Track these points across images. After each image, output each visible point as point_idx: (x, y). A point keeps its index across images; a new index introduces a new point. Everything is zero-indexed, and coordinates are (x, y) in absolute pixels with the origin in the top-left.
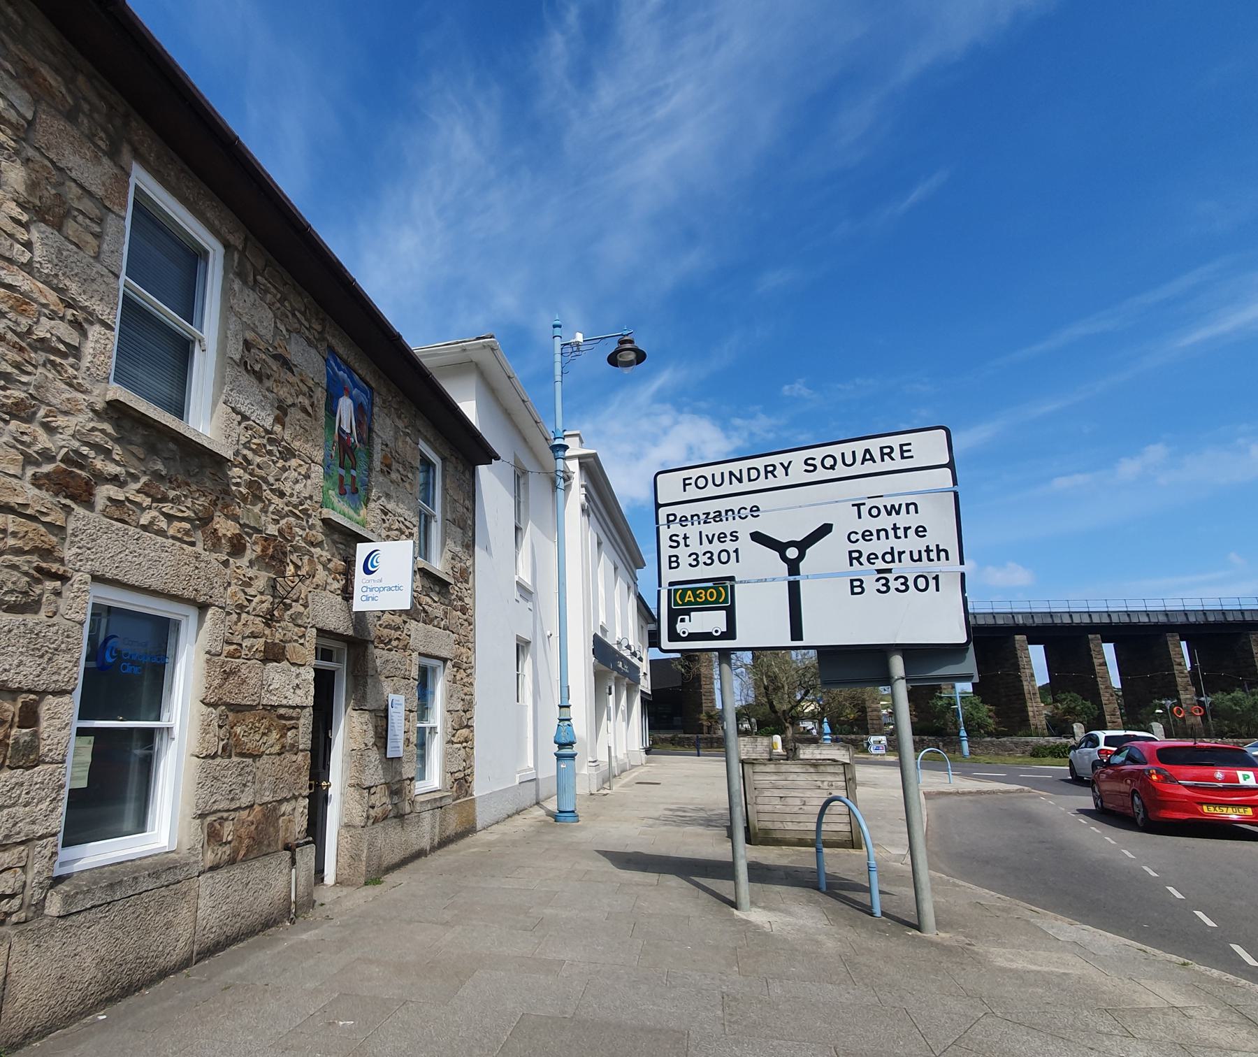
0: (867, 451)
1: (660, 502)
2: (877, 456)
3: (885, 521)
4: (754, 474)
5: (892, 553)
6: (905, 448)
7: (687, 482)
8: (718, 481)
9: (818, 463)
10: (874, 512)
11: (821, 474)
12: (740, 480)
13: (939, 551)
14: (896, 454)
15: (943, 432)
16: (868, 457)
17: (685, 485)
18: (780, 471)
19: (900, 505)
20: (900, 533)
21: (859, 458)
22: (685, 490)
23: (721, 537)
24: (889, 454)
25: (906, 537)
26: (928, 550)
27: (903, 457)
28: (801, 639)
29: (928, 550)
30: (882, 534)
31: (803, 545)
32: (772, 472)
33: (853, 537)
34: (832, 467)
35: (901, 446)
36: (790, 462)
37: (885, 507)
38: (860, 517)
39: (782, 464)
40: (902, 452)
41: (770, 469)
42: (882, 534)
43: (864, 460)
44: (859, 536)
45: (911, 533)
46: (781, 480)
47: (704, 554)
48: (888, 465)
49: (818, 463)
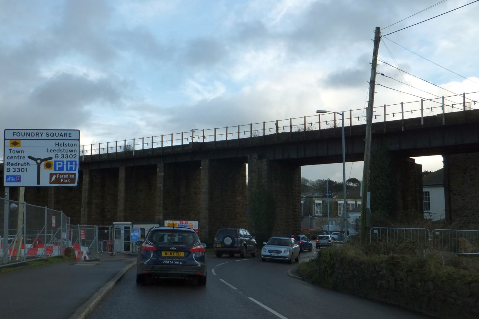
0: (61, 133)
1: (6, 138)
2: (63, 135)
3: (16, 155)
4: (33, 135)
5: (17, 164)
6: (70, 134)
7: (14, 133)
8: (23, 135)
9: (49, 134)
10: (14, 152)
11: (50, 138)
12: (29, 136)
13: (27, 163)
14: (68, 135)
15: (78, 131)
16: (61, 135)
17: (13, 134)
18: (40, 135)
19: (20, 151)
20: (19, 158)
21: (59, 135)
22: (13, 136)
23: (71, 151)
24: (66, 135)
25: (20, 159)
26: (25, 163)
27: (69, 136)
28: (40, 184)
29: (25, 163)
30: (15, 158)
31: (35, 160)
32: (38, 135)
33: (8, 158)
34: (53, 136)
35: (69, 133)
36: (43, 133)
37: (69, 150)
38: (10, 153)
39: (41, 133)
40: (69, 135)
41: (37, 134)
42: (15, 158)
43: (60, 136)
44: (10, 158)
45: (22, 158)
46: (40, 137)
47: (66, 155)
48: (66, 138)
49: (49, 134)
